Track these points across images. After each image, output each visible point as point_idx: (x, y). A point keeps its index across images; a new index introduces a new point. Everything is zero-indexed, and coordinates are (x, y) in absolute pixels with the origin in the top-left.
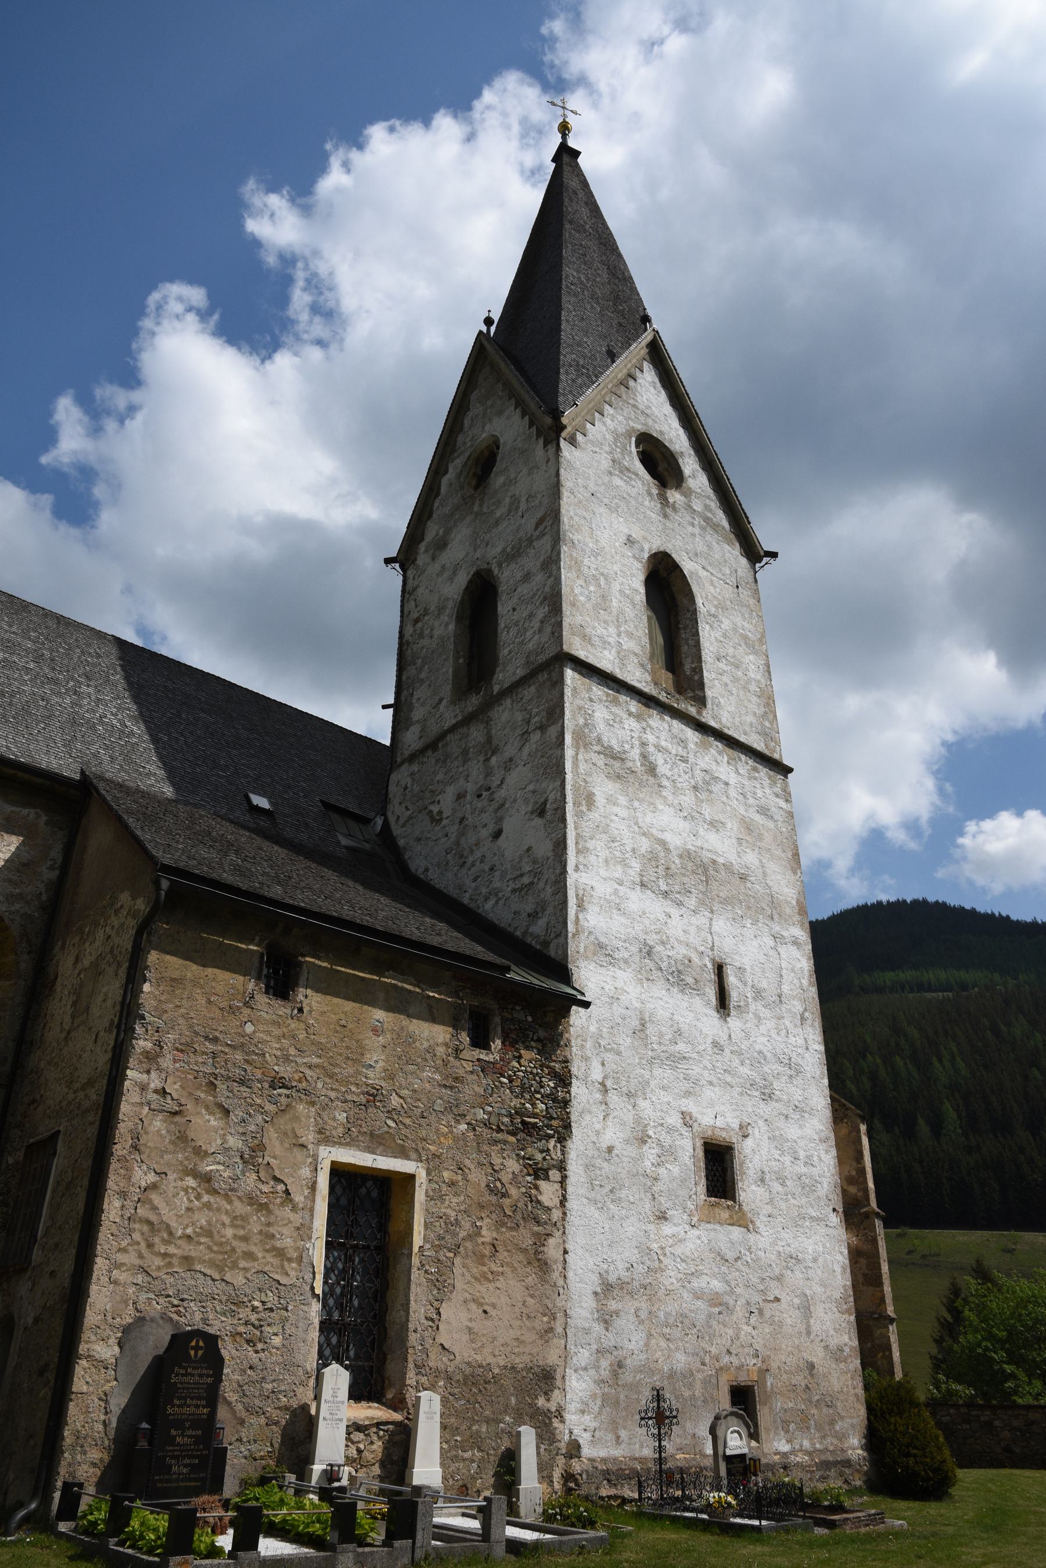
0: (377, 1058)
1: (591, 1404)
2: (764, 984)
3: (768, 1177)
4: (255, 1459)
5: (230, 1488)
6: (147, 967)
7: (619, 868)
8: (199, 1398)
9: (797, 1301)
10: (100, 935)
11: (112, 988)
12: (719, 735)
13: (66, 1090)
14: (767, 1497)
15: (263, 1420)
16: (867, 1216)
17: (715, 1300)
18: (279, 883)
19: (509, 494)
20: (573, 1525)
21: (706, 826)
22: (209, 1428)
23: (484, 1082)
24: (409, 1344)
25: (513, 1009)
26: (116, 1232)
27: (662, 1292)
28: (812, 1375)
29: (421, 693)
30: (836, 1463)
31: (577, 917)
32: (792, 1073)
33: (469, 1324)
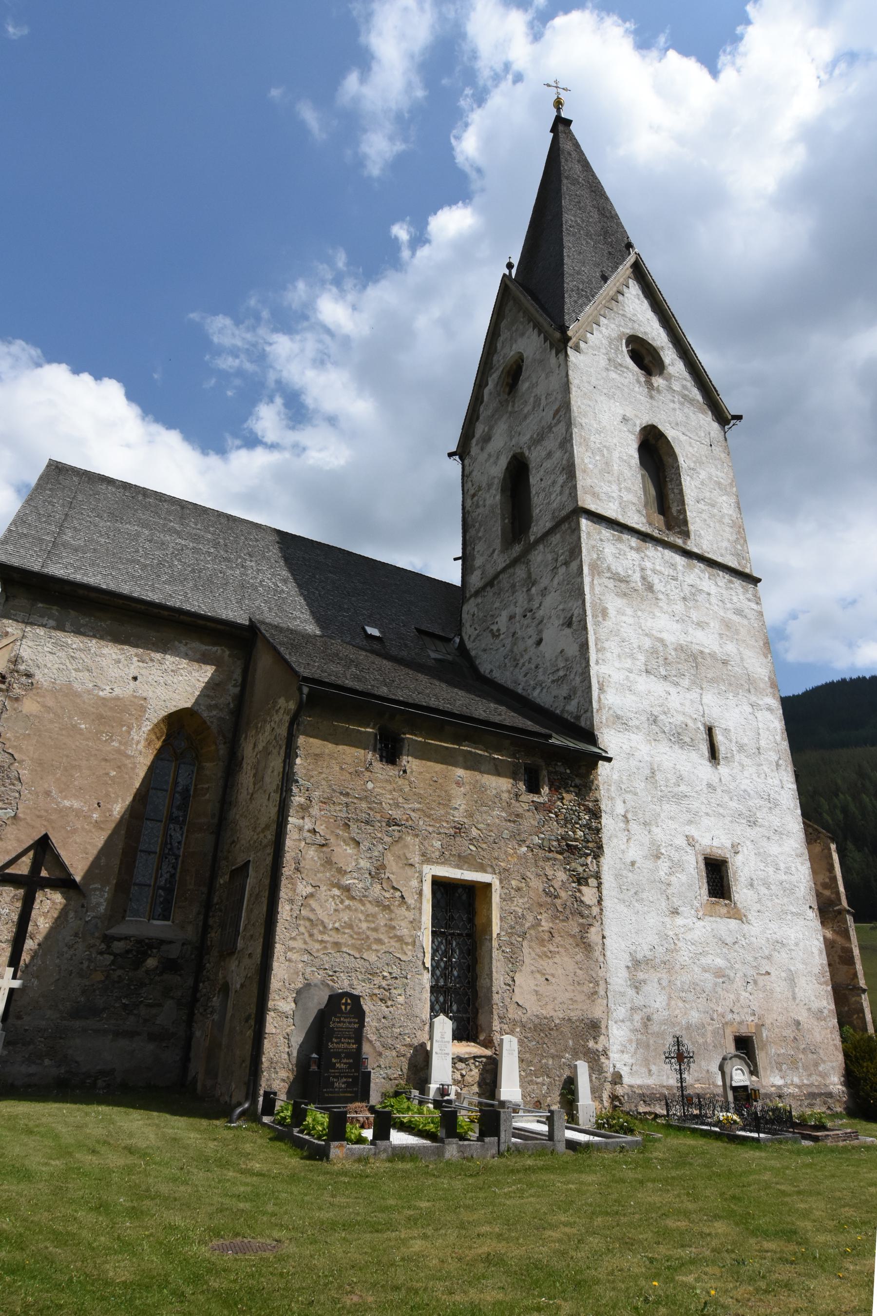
0: (460, 802)
1: (629, 1047)
2: (745, 740)
3: (756, 883)
4: (391, 1080)
5: (375, 1099)
6: (298, 747)
7: (629, 661)
8: (350, 1038)
9: (784, 975)
10: (268, 728)
11: (276, 763)
12: (711, 563)
13: (252, 833)
14: (762, 1118)
15: (394, 1053)
16: (840, 912)
17: (719, 973)
18: (386, 685)
19: (533, 395)
20: (617, 1132)
21: (694, 626)
22: (357, 1058)
23: (538, 817)
24: (494, 1002)
25: (556, 765)
26: (288, 927)
27: (677, 967)
28: (798, 1030)
29: (480, 547)
30: (820, 1095)
31: (599, 697)
32: (771, 805)
33: (536, 988)
